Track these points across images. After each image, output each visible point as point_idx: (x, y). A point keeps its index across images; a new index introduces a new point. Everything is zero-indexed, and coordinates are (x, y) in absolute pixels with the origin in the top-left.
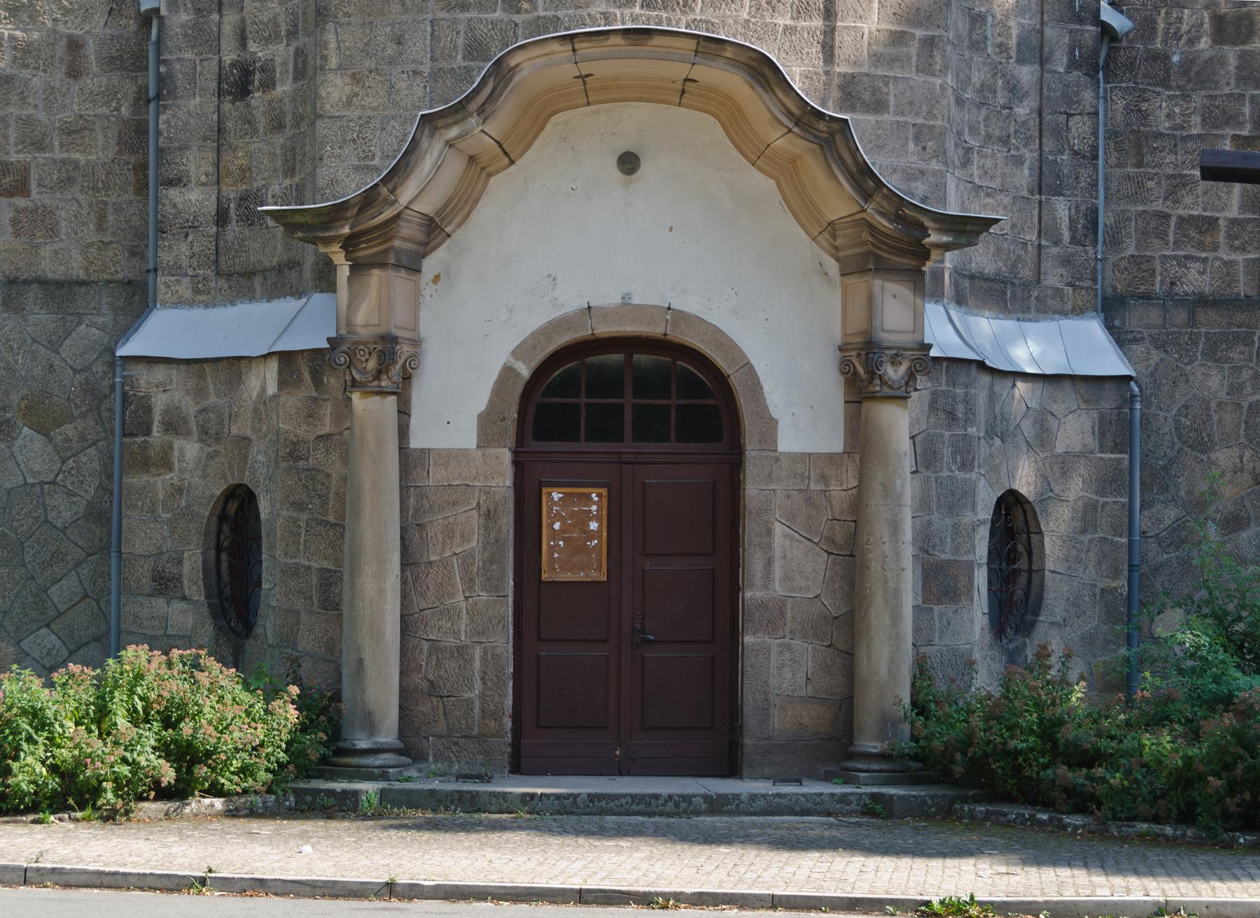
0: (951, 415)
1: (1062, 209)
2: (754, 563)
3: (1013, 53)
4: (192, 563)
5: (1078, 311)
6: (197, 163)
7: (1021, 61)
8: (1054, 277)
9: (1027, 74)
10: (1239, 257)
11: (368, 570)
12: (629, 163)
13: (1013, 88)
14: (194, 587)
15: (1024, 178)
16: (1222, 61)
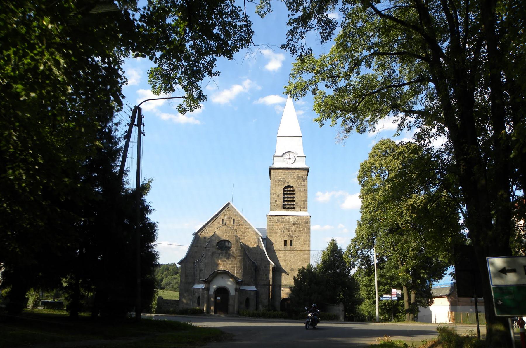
4: (196, 301)
5: (253, 286)
6: (198, 275)
12: (222, 277)
14: (197, 303)
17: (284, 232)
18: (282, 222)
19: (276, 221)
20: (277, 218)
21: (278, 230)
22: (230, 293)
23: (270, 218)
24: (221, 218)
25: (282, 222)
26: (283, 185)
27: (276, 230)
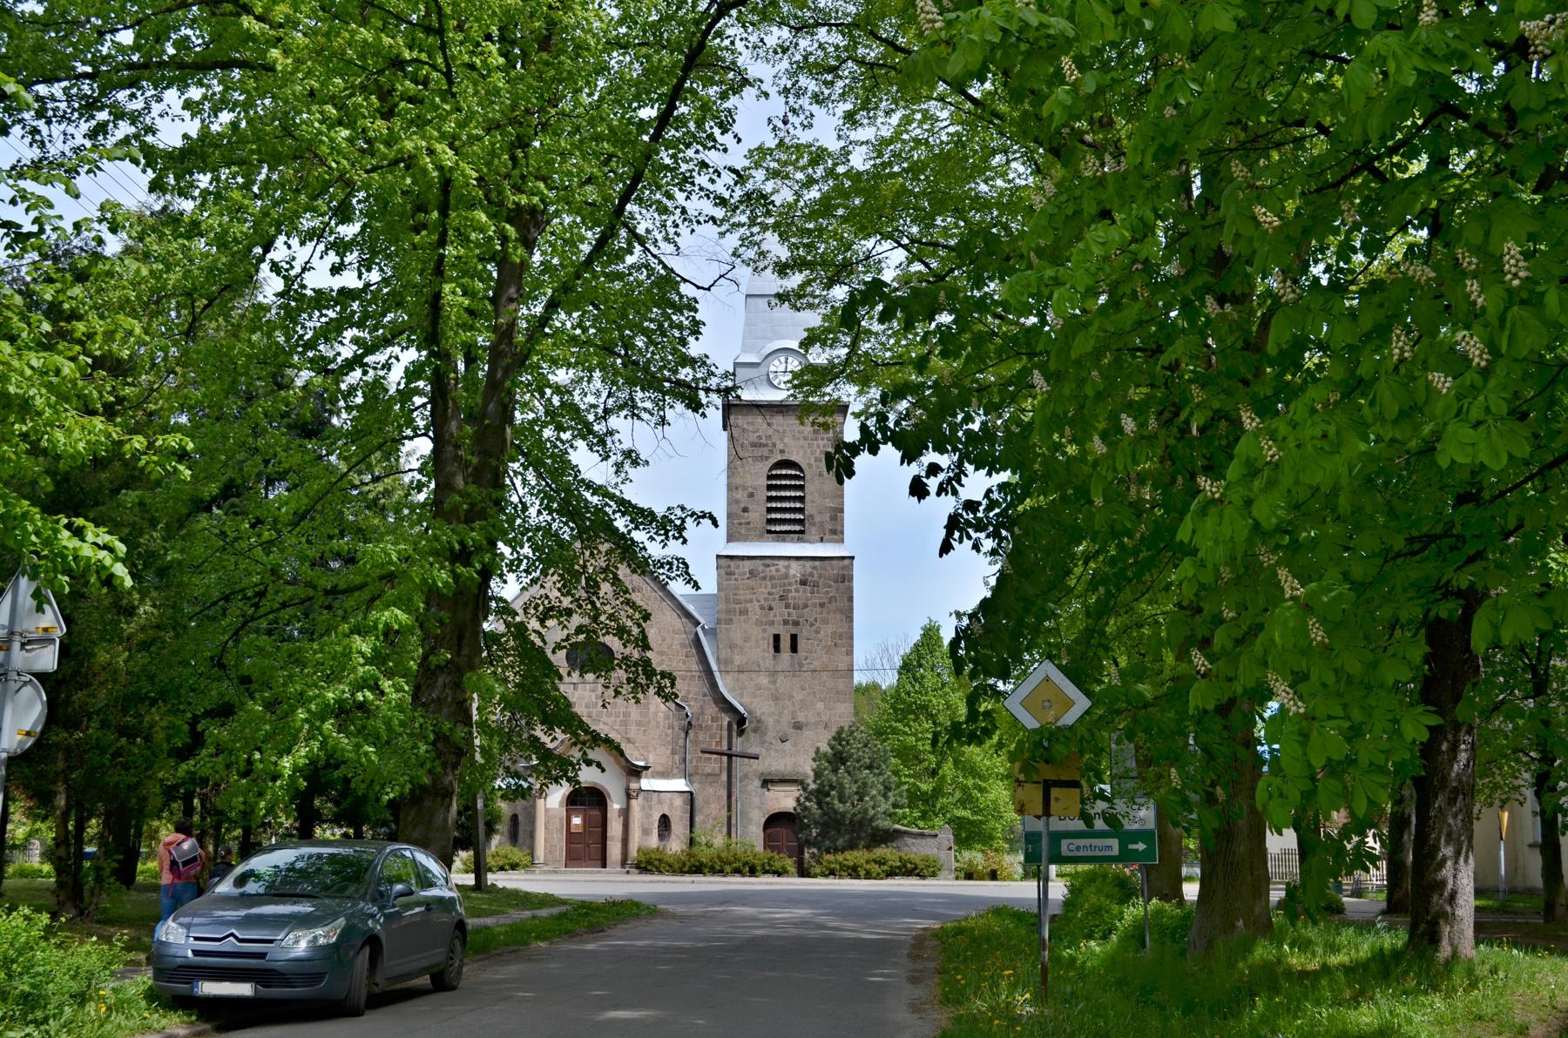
17: (771, 609)
18: (764, 578)
25: (764, 578)
27: (747, 601)
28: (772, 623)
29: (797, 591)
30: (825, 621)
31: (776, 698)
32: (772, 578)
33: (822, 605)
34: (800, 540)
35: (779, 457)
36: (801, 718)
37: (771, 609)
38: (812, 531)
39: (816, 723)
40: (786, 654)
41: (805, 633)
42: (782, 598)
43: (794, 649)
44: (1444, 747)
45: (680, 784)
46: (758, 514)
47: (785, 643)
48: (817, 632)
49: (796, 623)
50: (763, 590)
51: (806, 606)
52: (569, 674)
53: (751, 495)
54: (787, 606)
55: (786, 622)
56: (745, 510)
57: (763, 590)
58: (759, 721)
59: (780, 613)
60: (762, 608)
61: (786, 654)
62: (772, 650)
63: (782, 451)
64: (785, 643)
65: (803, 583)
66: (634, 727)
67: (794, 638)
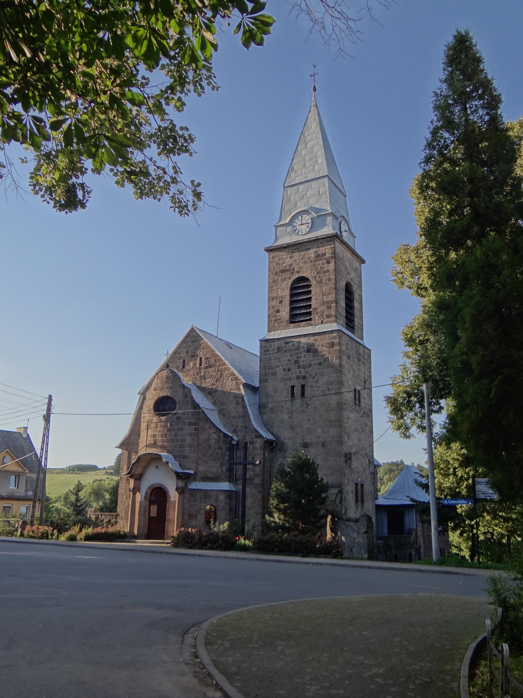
0: (193, 496)
1: (224, 468)
2: (167, 514)
3: (217, 449)
5: (226, 481)
7: (218, 449)
8: (223, 477)
9: (219, 451)
10: (252, 473)
11: (171, 511)
12: (157, 467)
13: (217, 454)
15: (219, 464)
16: (250, 447)
17: (289, 370)
18: (286, 351)
19: (274, 350)
20: (276, 343)
21: (278, 367)
22: (170, 497)
23: (266, 347)
24: (180, 358)
25: (286, 351)
26: (290, 278)
28: (290, 379)
29: (305, 356)
30: (322, 374)
31: (292, 428)
32: (290, 350)
33: (320, 364)
34: (309, 325)
35: (296, 276)
36: (307, 440)
37: (289, 370)
38: (315, 317)
39: (317, 443)
40: (298, 401)
41: (309, 384)
42: (296, 362)
43: (303, 395)
44: (476, 549)
45: (225, 486)
46: (285, 313)
47: (297, 391)
48: (317, 382)
49: (304, 378)
50: (285, 358)
51: (310, 366)
52: (488, 529)
53: (281, 302)
54: (299, 367)
55: (298, 378)
56: (278, 311)
57: (285, 358)
58: (283, 444)
59: (295, 371)
60: (284, 370)
61: (298, 401)
62: (290, 396)
63: (298, 272)
64: (297, 391)
65: (308, 351)
66: (187, 449)
67: (303, 386)
